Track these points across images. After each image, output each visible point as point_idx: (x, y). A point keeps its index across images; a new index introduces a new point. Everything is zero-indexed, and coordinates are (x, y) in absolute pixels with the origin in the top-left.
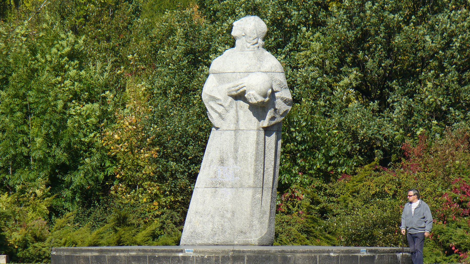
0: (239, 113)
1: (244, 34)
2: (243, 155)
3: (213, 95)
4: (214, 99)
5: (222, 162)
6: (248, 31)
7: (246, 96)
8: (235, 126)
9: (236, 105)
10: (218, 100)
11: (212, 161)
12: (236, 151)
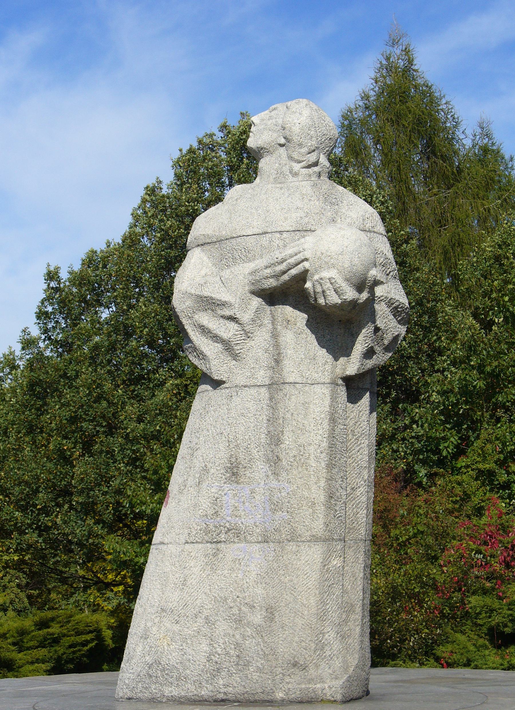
0: (281, 339)
1: (283, 141)
2: (294, 452)
3: (206, 294)
4: (209, 304)
5: (234, 472)
6: (296, 129)
7: (308, 285)
8: (269, 373)
9: (273, 317)
10: (223, 304)
11: (205, 470)
12: (275, 439)
